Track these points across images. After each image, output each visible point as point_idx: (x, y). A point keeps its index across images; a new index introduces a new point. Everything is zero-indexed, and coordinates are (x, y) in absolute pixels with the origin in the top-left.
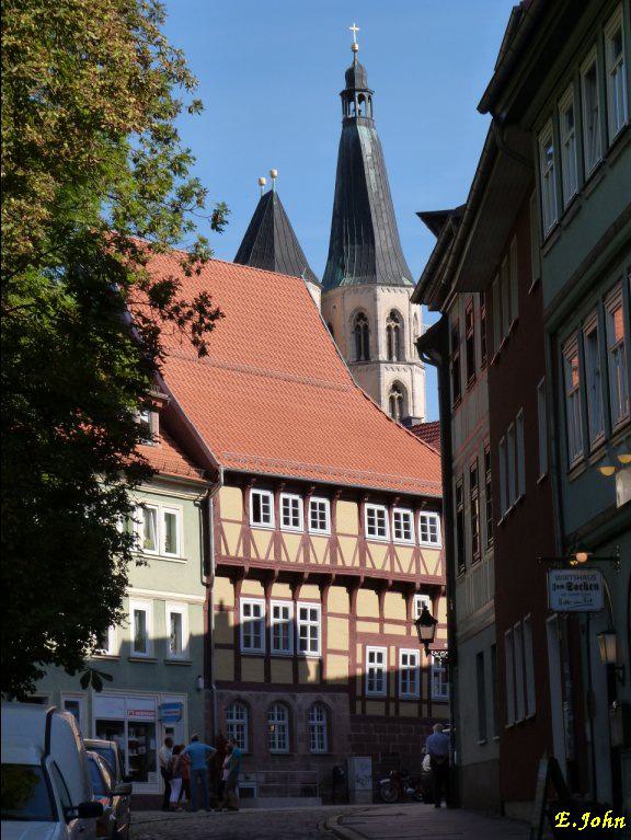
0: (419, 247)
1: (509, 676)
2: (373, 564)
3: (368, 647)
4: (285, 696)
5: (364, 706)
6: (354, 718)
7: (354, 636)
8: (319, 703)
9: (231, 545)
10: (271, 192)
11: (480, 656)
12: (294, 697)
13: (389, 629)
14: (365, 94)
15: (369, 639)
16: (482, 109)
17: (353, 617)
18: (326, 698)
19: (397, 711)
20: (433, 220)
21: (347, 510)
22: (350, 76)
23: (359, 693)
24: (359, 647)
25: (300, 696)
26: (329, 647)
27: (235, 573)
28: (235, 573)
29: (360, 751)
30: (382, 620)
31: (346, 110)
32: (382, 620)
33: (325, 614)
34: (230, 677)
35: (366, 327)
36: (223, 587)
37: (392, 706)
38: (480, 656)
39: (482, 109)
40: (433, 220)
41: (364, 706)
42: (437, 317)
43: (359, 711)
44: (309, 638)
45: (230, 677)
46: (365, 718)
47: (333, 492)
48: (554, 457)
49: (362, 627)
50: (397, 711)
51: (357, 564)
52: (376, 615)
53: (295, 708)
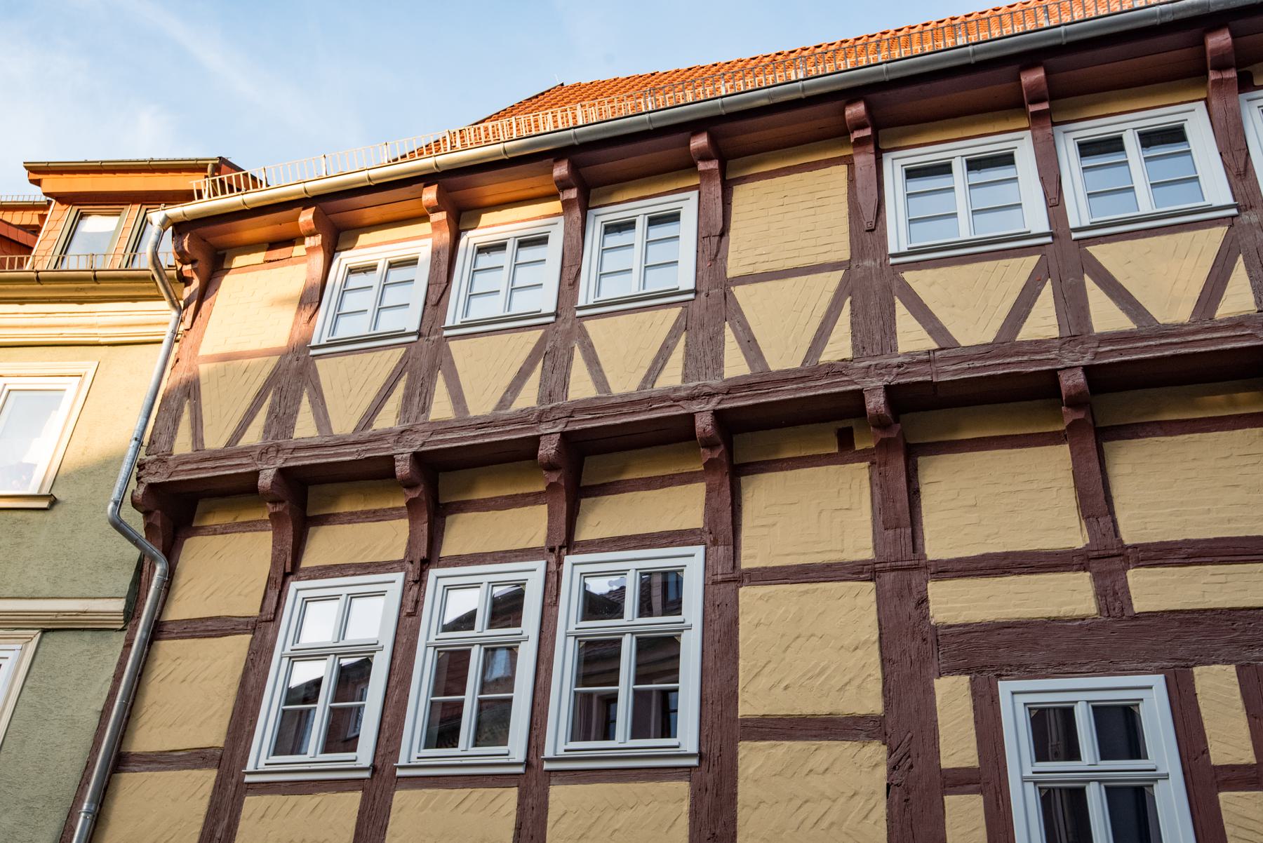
2: (523, 375)
3: (1005, 688)
7: (913, 647)
13: (1151, 590)
15: (990, 653)
24: (952, 696)
26: (753, 701)
33: (728, 579)
49: (952, 603)
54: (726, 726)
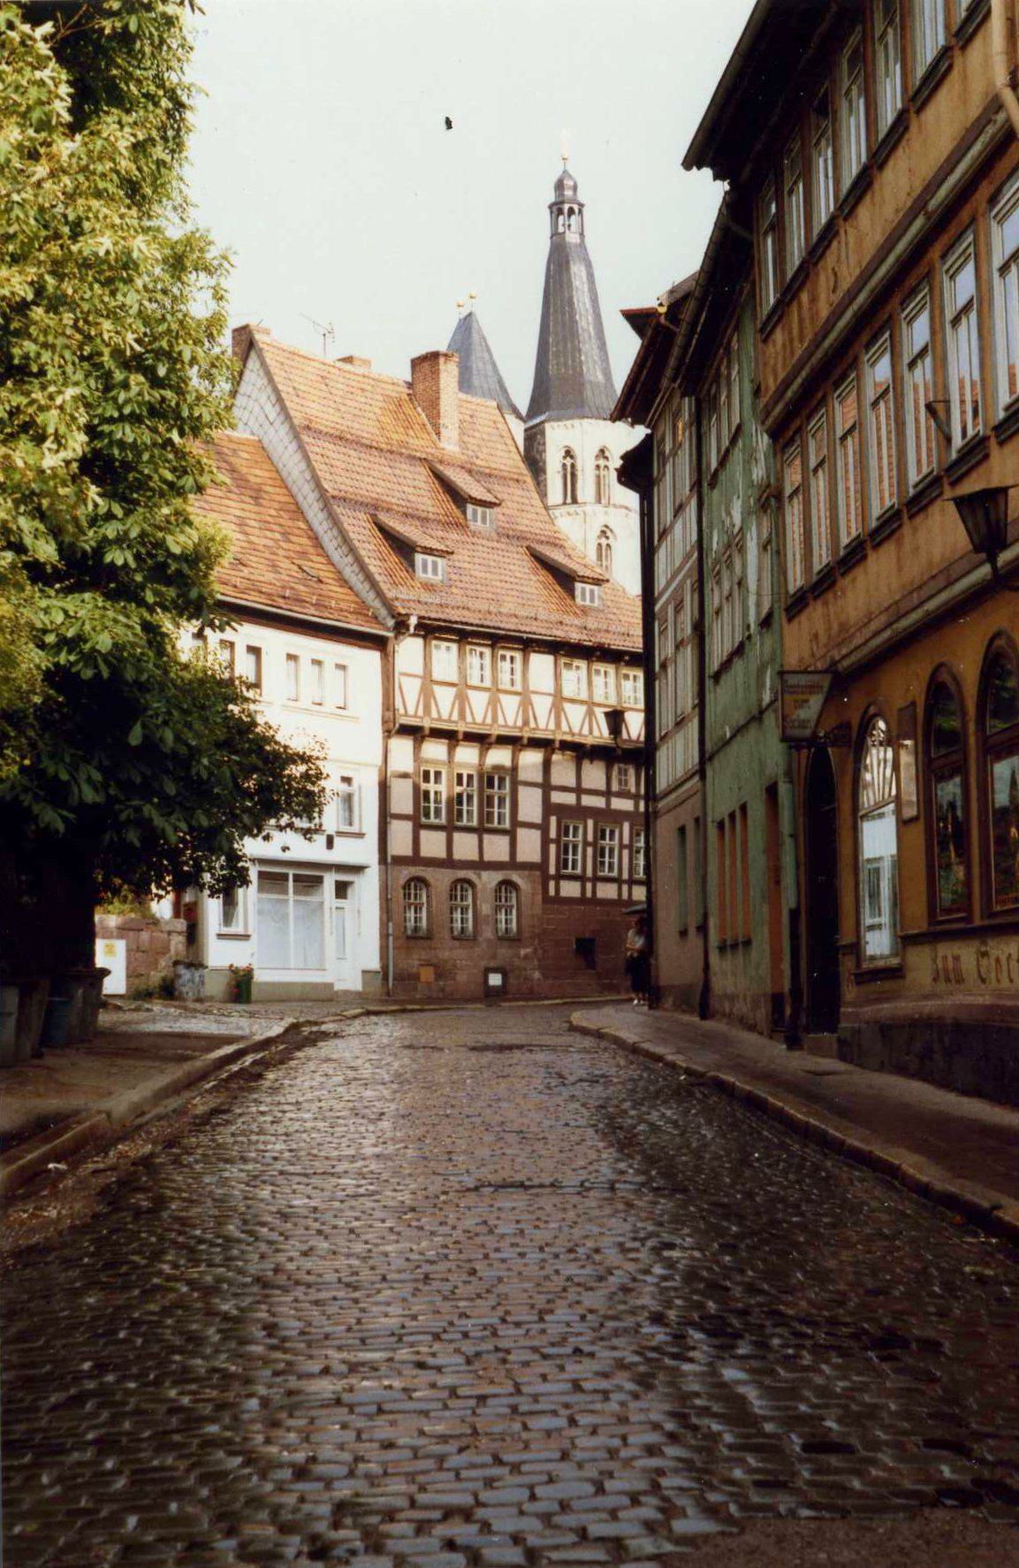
0: (625, 348)
1: (873, 462)
4: (471, 875)
5: (620, 894)
6: (546, 899)
7: (548, 808)
8: (507, 884)
9: (410, 706)
10: (470, 314)
11: (682, 830)
12: (479, 876)
14: (576, 208)
15: (561, 810)
16: (694, 159)
17: (547, 787)
18: (515, 877)
19: (594, 892)
20: (638, 319)
21: (542, 663)
22: (560, 186)
23: (552, 871)
24: (553, 819)
25: (485, 875)
26: (521, 817)
27: (414, 732)
28: (414, 732)
29: (58, 654)
30: (579, 790)
31: (555, 224)
32: (579, 790)
34: (408, 852)
35: (573, 466)
36: (402, 749)
37: (589, 886)
38: (682, 830)
39: (694, 159)
40: (638, 319)
41: (620, 894)
42: (641, 432)
43: (552, 892)
44: (432, 805)
45: (408, 852)
46: (559, 900)
47: (528, 645)
48: (728, 862)
49: (557, 798)
50: (594, 892)
51: (552, 726)
52: (603, 787)
53: (479, 886)
54: (516, 824)
